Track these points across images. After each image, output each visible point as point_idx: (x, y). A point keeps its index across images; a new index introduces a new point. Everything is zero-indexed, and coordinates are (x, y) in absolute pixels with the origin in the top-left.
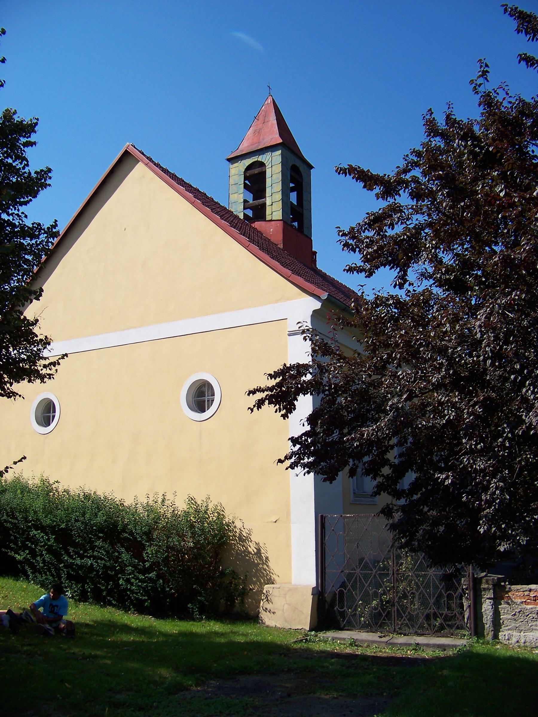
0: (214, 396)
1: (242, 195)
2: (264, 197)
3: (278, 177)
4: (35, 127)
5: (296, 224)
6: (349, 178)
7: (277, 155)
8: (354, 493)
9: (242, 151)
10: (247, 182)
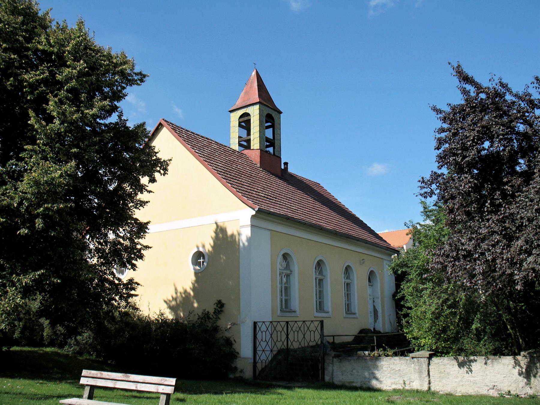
1: (238, 134)
3: (257, 123)
4: (125, 96)
5: (271, 149)
6: (146, 222)
7: (257, 107)
9: (238, 106)
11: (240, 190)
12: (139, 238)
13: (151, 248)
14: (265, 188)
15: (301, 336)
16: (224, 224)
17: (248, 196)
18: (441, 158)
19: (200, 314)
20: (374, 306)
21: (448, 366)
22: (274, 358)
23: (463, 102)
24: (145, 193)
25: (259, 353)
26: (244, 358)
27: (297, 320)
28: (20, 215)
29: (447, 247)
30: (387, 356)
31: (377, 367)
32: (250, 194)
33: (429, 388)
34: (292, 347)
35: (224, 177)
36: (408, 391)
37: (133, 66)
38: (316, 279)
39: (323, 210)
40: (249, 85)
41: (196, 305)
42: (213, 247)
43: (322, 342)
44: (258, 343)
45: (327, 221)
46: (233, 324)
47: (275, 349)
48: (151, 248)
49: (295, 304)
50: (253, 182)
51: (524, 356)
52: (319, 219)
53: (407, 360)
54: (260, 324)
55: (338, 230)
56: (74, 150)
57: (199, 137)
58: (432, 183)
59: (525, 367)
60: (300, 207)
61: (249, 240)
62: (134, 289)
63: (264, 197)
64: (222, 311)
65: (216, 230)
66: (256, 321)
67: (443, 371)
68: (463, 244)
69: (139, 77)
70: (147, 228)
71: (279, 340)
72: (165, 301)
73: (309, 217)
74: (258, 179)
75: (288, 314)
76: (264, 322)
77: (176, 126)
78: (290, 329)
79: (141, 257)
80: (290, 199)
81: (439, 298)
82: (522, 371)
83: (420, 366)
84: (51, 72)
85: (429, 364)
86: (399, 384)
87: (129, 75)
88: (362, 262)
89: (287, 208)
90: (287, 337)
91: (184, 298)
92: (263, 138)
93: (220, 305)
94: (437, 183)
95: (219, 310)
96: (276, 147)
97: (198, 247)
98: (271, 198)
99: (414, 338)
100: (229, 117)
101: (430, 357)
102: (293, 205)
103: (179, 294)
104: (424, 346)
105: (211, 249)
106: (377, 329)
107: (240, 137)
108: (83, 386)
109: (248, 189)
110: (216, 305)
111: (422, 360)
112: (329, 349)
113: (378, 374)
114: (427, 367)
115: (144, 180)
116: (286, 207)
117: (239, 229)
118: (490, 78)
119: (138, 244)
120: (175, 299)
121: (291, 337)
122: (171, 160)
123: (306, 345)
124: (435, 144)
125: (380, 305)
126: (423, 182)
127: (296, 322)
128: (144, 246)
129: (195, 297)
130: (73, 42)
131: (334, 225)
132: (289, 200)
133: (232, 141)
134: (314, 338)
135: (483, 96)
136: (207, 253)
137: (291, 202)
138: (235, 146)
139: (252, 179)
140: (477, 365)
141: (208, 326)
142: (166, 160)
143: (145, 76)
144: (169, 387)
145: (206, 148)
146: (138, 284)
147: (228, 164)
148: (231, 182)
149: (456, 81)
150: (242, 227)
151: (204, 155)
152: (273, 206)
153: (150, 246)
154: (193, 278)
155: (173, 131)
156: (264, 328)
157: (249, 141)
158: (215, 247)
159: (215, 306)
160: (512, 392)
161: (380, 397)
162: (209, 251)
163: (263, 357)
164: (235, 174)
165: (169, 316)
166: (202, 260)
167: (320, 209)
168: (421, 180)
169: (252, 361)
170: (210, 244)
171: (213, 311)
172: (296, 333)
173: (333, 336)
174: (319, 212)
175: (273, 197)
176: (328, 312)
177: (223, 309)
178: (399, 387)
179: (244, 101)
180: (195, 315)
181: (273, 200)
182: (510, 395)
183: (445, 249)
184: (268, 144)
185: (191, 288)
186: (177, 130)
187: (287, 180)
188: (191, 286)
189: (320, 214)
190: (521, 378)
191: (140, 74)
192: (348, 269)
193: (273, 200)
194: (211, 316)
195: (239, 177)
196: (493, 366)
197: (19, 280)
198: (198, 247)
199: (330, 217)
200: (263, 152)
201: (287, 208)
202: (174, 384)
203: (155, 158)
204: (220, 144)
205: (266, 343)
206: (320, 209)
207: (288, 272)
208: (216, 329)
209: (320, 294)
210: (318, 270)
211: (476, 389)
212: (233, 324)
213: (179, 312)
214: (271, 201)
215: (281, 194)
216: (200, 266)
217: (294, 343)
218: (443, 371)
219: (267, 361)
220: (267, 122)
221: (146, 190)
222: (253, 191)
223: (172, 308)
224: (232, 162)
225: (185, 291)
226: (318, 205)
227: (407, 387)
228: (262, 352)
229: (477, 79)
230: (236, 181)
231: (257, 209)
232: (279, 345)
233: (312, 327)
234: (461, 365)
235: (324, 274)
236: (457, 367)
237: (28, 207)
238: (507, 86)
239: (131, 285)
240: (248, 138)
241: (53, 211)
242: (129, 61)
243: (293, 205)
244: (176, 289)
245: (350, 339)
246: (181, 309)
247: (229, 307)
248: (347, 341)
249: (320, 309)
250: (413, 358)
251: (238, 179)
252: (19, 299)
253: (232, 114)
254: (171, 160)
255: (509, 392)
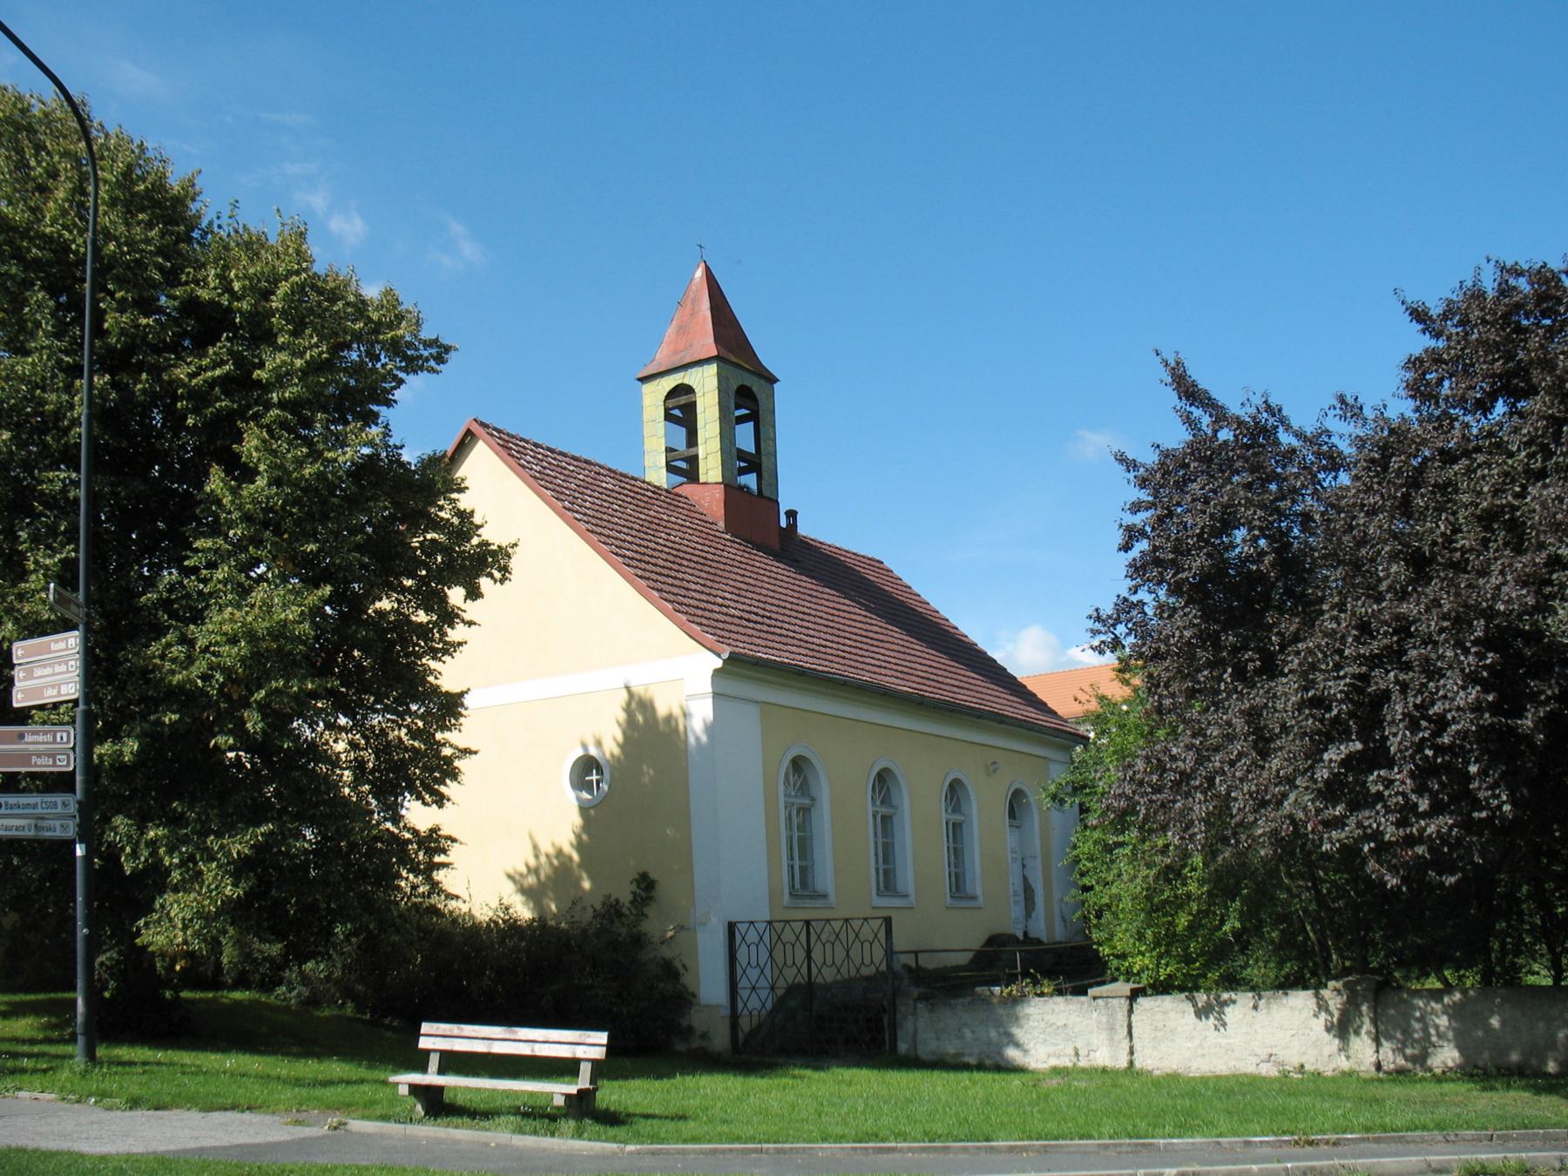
1: (663, 441)
5: (750, 480)
7: (712, 369)
11: (681, 604)
12: (444, 728)
13: (476, 753)
14: (743, 593)
15: (840, 953)
16: (646, 690)
17: (704, 621)
18: (1137, 569)
19: (598, 906)
20: (1025, 879)
21: (1173, 1015)
22: (780, 1004)
23: (1191, 438)
24: (460, 627)
25: (744, 994)
26: (708, 1006)
27: (830, 917)
28: (211, 704)
29: (1140, 765)
30: (1042, 995)
31: (1017, 1018)
32: (707, 614)
33: (1131, 1063)
34: (820, 980)
35: (640, 572)
36: (1084, 1070)
37: (418, 324)
38: (874, 816)
39: (891, 639)
40: (689, 306)
41: (587, 885)
42: (622, 747)
43: (888, 966)
44: (739, 971)
45: (900, 668)
46: (680, 928)
47: (781, 983)
48: (476, 753)
49: (826, 877)
50: (711, 577)
51: (1335, 989)
52: (880, 667)
53: (1083, 1003)
54: (742, 928)
55: (929, 692)
56: (311, 547)
57: (567, 460)
58: (1118, 621)
59: (1336, 1014)
60: (831, 638)
61: (710, 729)
62: (444, 851)
63: (741, 618)
64: (651, 898)
65: (629, 704)
66: (734, 920)
67: (1160, 1025)
68: (1174, 758)
69: (434, 351)
70: (462, 705)
71: (789, 963)
72: (510, 877)
73: (853, 663)
74: (722, 566)
75: (808, 903)
76: (752, 923)
77: (508, 435)
79: (454, 774)
80: (806, 617)
81: (1149, 866)
82: (1332, 1023)
83: (1112, 1015)
84: (239, 360)
85: (1131, 1011)
86: (1065, 1055)
87: (410, 345)
88: (992, 769)
89: (798, 643)
90: (809, 957)
91: (555, 869)
92: (730, 453)
93: (646, 884)
94: (1129, 621)
95: (644, 895)
96: (765, 475)
97: (584, 746)
98: (759, 619)
99: (1117, 957)
100: (640, 396)
101: (1134, 995)
102: (812, 632)
103: (543, 859)
104: (1138, 973)
105: (617, 751)
106: (1032, 935)
107: (669, 450)
108: (427, 1052)
109: (699, 600)
110: (635, 884)
111: (1115, 1001)
112: (906, 981)
113: (1018, 1032)
114: (1126, 1019)
115: (456, 595)
116: (795, 642)
117: (684, 704)
118: (1244, 399)
119: (444, 745)
120: (535, 871)
121: (817, 955)
122: (516, 545)
123: (853, 972)
124: (1118, 538)
125: (1040, 875)
126: (1098, 619)
127: (828, 920)
128: (460, 750)
129: (581, 865)
130: (284, 288)
132: (802, 620)
133: (648, 461)
134: (871, 959)
135: (1225, 435)
136: (608, 761)
137: (807, 624)
138: (658, 476)
139: (707, 569)
140: (1236, 1013)
141: (619, 935)
142: (504, 545)
143: (447, 349)
144: (597, 1048)
145: (588, 492)
146: (454, 840)
147: (646, 533)
148: (659, 586)
149: (1172, 397)
150: (691, 697)
151: (585, 514)
152: (763, 643)
153: (474, 749)
154: (577, 820)
155: (504, 453)
156: (752, 937)
157: (693, 461)
158: (628, 744)
159: (634, 887)
160: (1307, 1067)
161: (1015, 1081)
162: (612, 755)
163: (754, 1003)
164: (666, 560)
165: (524, 912)
166: (594, 777)
167: (881, 637)
168: (1095, 614)
169: (727, 1012)
170: (615, 739)
171: (631, 897)
172: (828, 946)
173: (916, 953)
174: (881, 644)
175: (763, 616)
176: (906, 896)
177: (654, 893)
178: (1066, 1062)
179: (676, 352)
180: (585, 909)
181: (762, 624)
182: (1303, 1073)
183: (1136, 768)
184: (742, 464)
185: (572, 845)
186: (511, 447)
187: (797, 561)
188: (572, 837)
189: (883, 651)
190: (1327, 1037)
191: (434, 343)
192: (955, 791)
193: (762, 624)
194: (625, 911)
195: (675, 567)
196: (1269, 1012)
197: (222, 847)
198: (584, 746)
199: (909, 658)
200: (732, 490)
201: (798, 643)
202: (605, 1041)
203: (475, 541)
204: (621, 475)
205: (757, 971)
206: (881, 637)
207: (807, 801)
208: (638, 941)
209: (887, 853)
210: (880, 792)
211: (1232, 1064)
212: (680, 928)
213: (546, 901)
214: (758, 627)
215: (783, 604)
216: (590, 791)
217: (825, 971)
218: (1160, 1025)
219: (764, 1012)
220: (738, 407)
221: (463, 621)
222: (714, 604)
223: (527, 892)
224: (654, 526)
225: (560, 853)
226: (877, 624)
227: (1083, 1063)
229: (1217, 394)
230: (670, 581)
231: (725, 656)
232: (790, 974)
233: (866, 933)
234: (1202, 1013)
235: (895, 802)
236: (1193, 1015)
237: (222, 686)
238: (1280, 410)
239: (434, 842)
240: (692, 451)
241: (288, 695)
242: (408, 312)
243: (812, 632)
244: (535, 847)
245: (963, 959)
246: (551, 894)
247: (666, 888)
248: (954, 964)
249: (887, 888)
250: (1095, 998)
251: (673, 573)
252: (229, 888)
253: (648, 388)
254: (516, 545)
255: (1302, 1066)
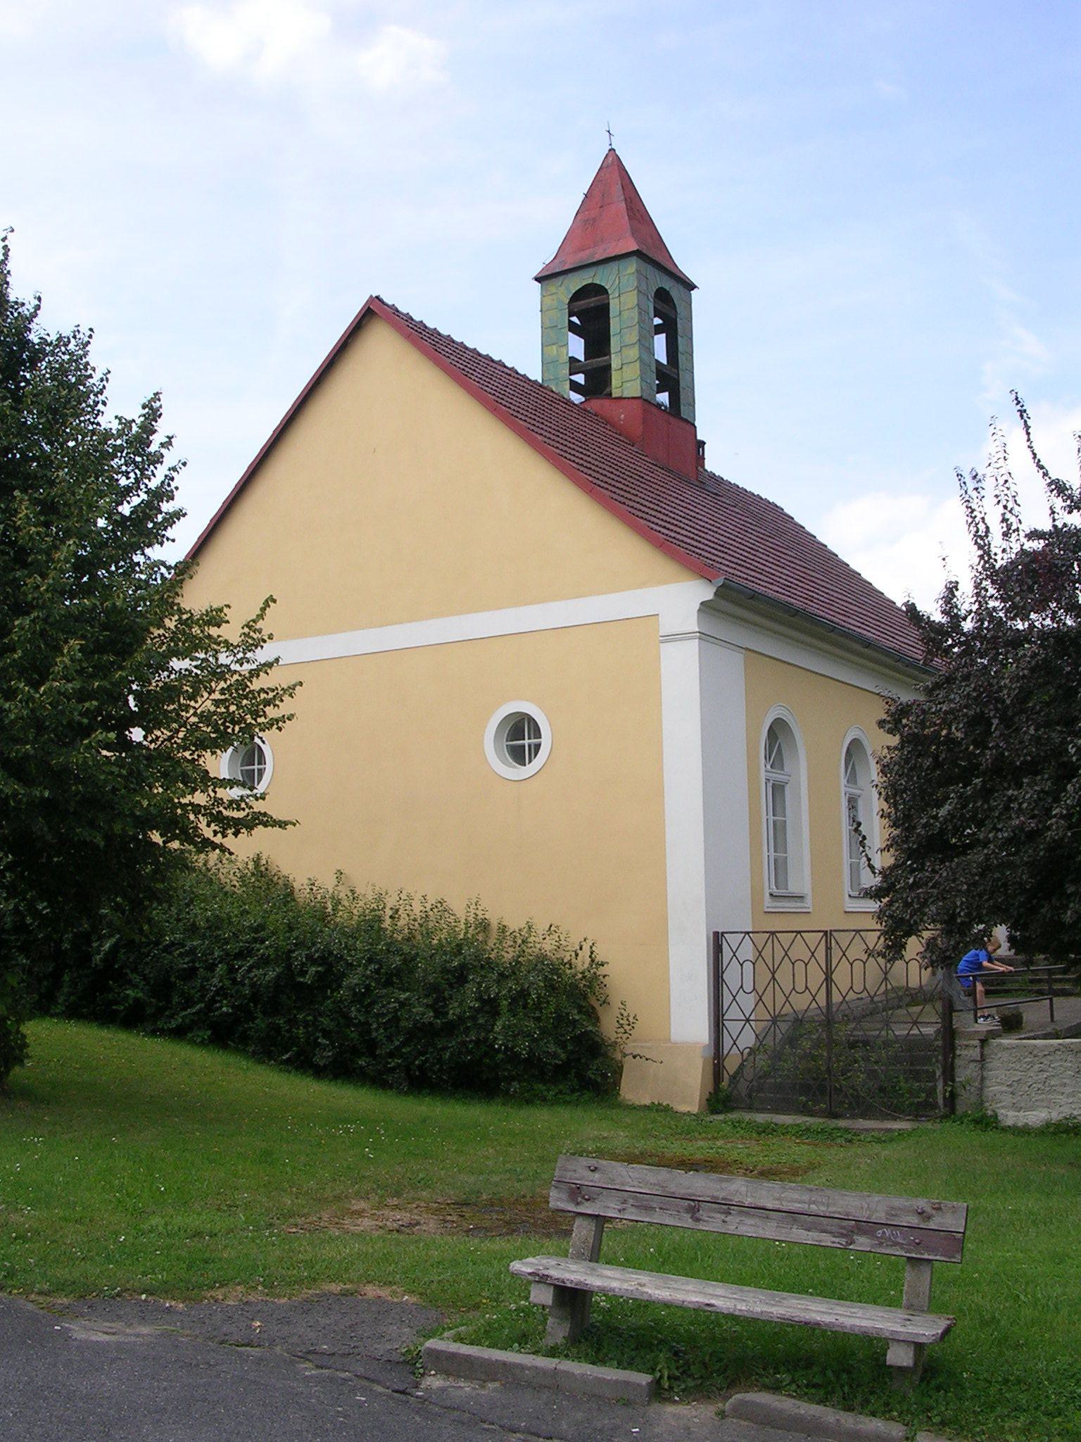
0: (540, 738)
2: (609, 353)
5: (663, 398)
8: (771, 895)
10: (575, 319)
25: (732, 1027)
49: (801, 881)
78: (836, 954)
90: (828, 979)
131: (879, 633)
228: (747, 1024)
233: (799, 951)
